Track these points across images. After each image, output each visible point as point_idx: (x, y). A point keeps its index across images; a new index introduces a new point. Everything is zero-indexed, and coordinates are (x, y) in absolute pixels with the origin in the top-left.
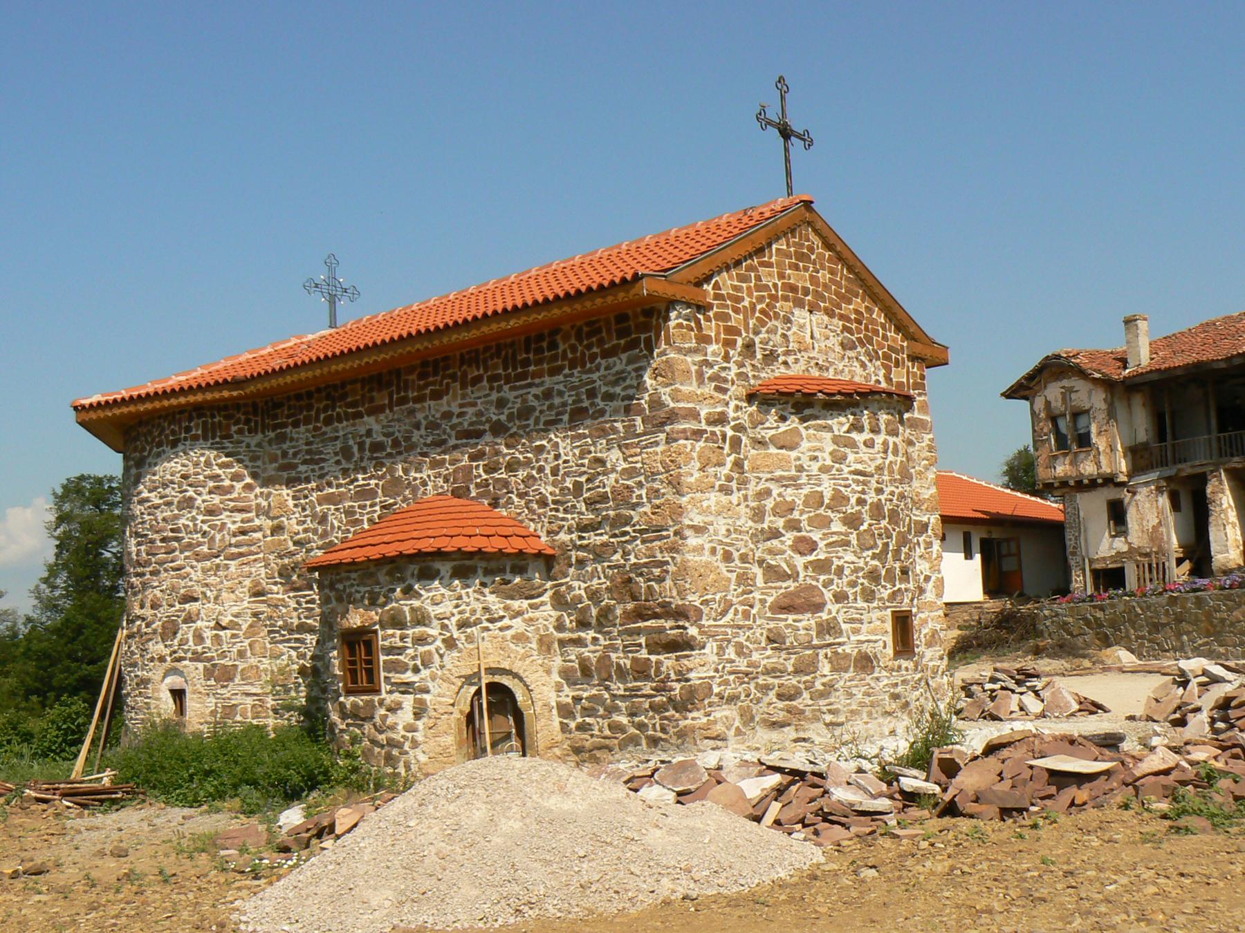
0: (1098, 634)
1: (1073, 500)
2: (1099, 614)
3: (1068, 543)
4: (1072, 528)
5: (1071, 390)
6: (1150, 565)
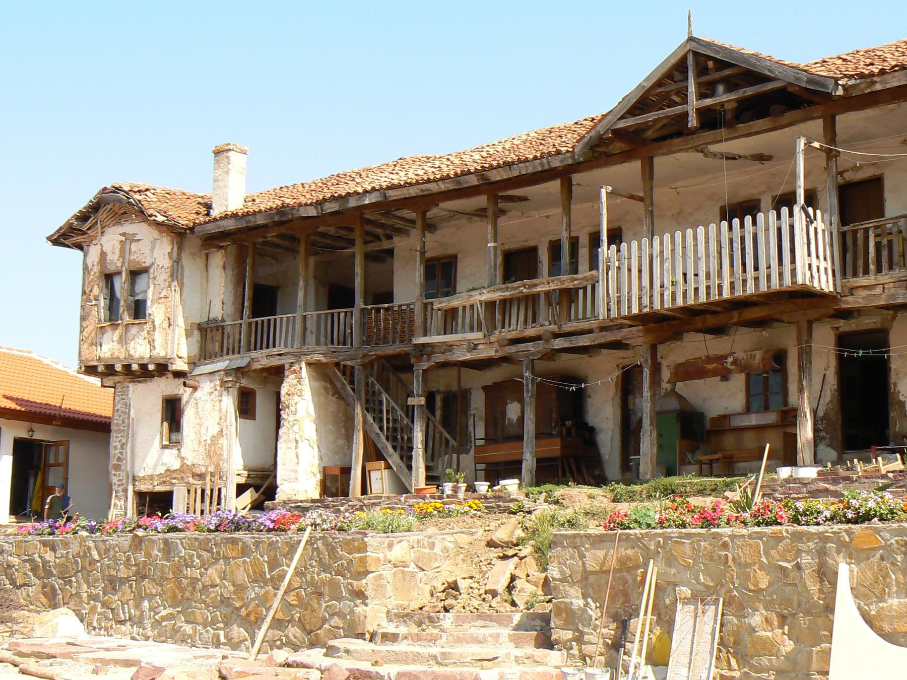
0: (44, 586)
1: (125, 393)
2: (49, 556)
3: (112, 452)
4: (119, 431)
5: (130, 239)
6: (203, 491)
